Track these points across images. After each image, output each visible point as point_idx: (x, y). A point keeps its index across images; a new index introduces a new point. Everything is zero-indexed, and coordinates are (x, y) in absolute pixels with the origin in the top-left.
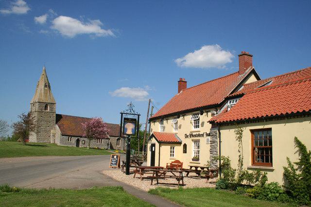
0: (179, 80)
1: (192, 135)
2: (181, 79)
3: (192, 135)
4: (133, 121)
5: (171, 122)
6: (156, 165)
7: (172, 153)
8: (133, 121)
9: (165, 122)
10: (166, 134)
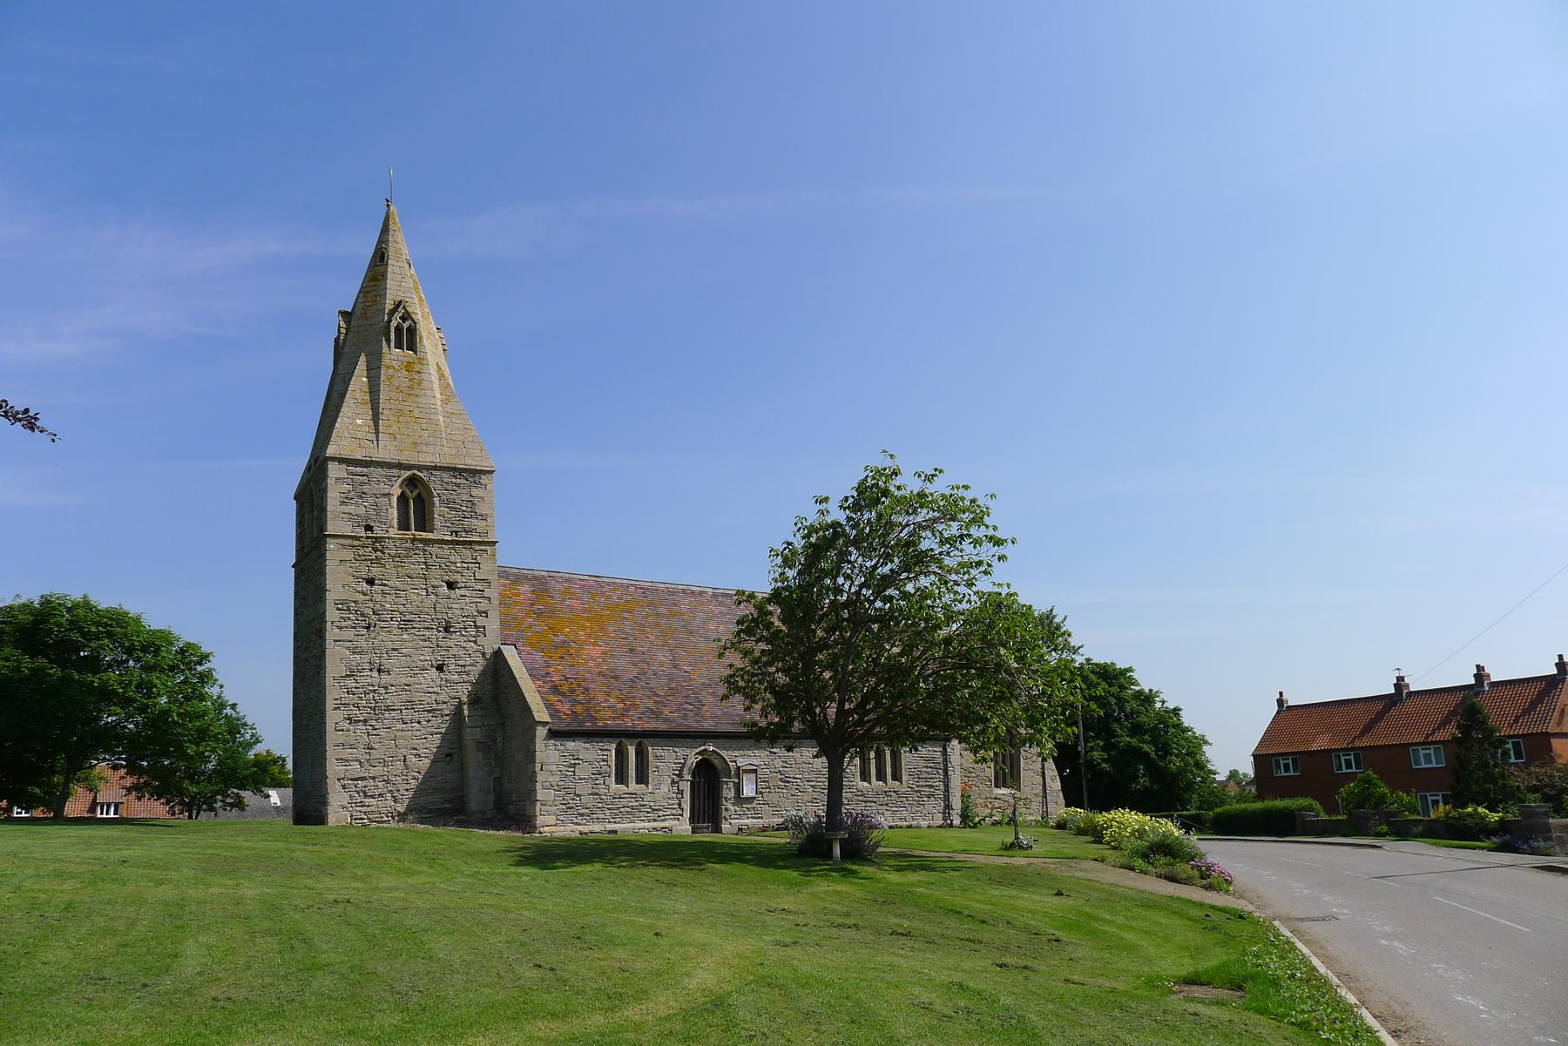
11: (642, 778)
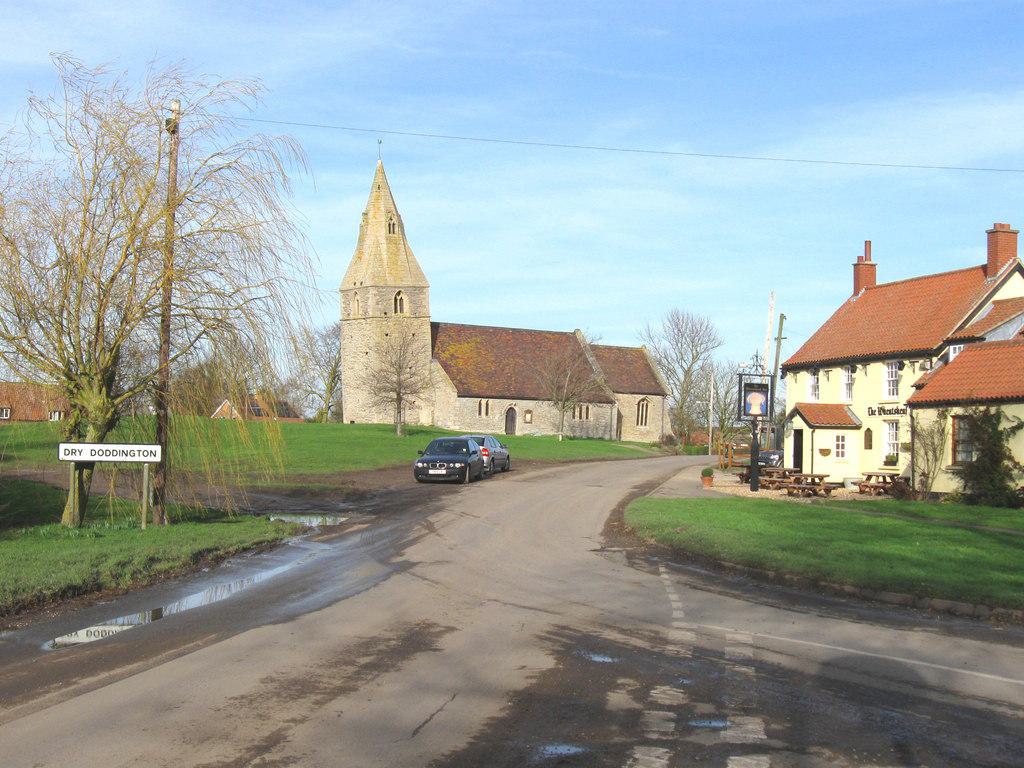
0: (856, 262)
1: (882, 411)
2: (866, 448)
3: (882, 411)
4: (761, 388)
5: (839, 374)
6: (806, 470)
7: (840, 450)
8: (761, 388)
9: (821, 373)
10: (826, 407)
11: (487, 414)
